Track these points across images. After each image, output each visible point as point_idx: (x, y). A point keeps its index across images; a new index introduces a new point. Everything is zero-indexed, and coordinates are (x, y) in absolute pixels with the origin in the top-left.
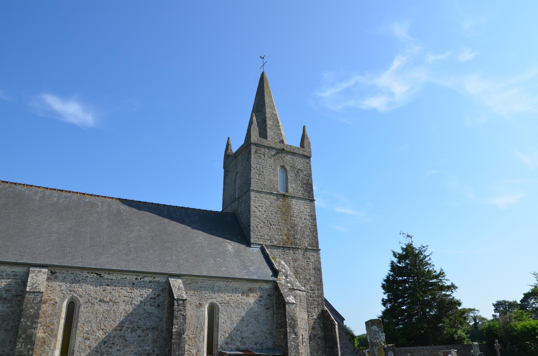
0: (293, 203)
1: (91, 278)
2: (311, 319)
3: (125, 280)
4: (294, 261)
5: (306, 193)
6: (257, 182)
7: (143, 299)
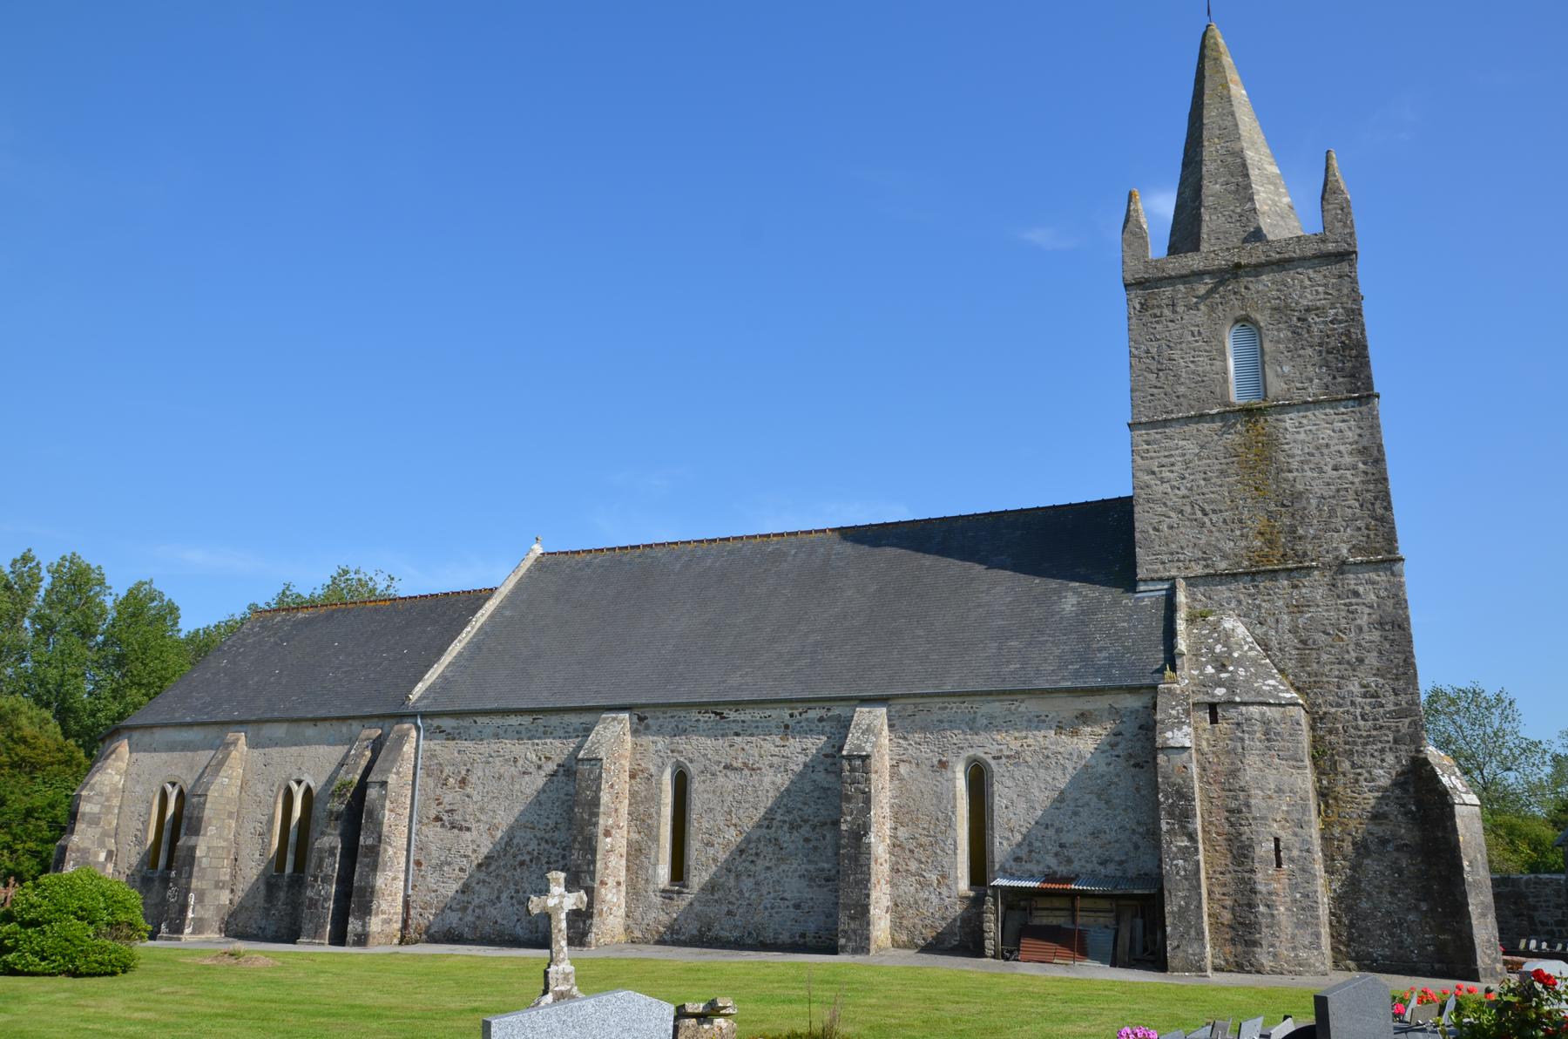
0: (1287, 425)
1: (706, 722)
2: (1366, 789)
3: (769, 721)
4: (1296, 610)
5: (1341, 380)
6: (1152, 395)
7: (808, 760)
